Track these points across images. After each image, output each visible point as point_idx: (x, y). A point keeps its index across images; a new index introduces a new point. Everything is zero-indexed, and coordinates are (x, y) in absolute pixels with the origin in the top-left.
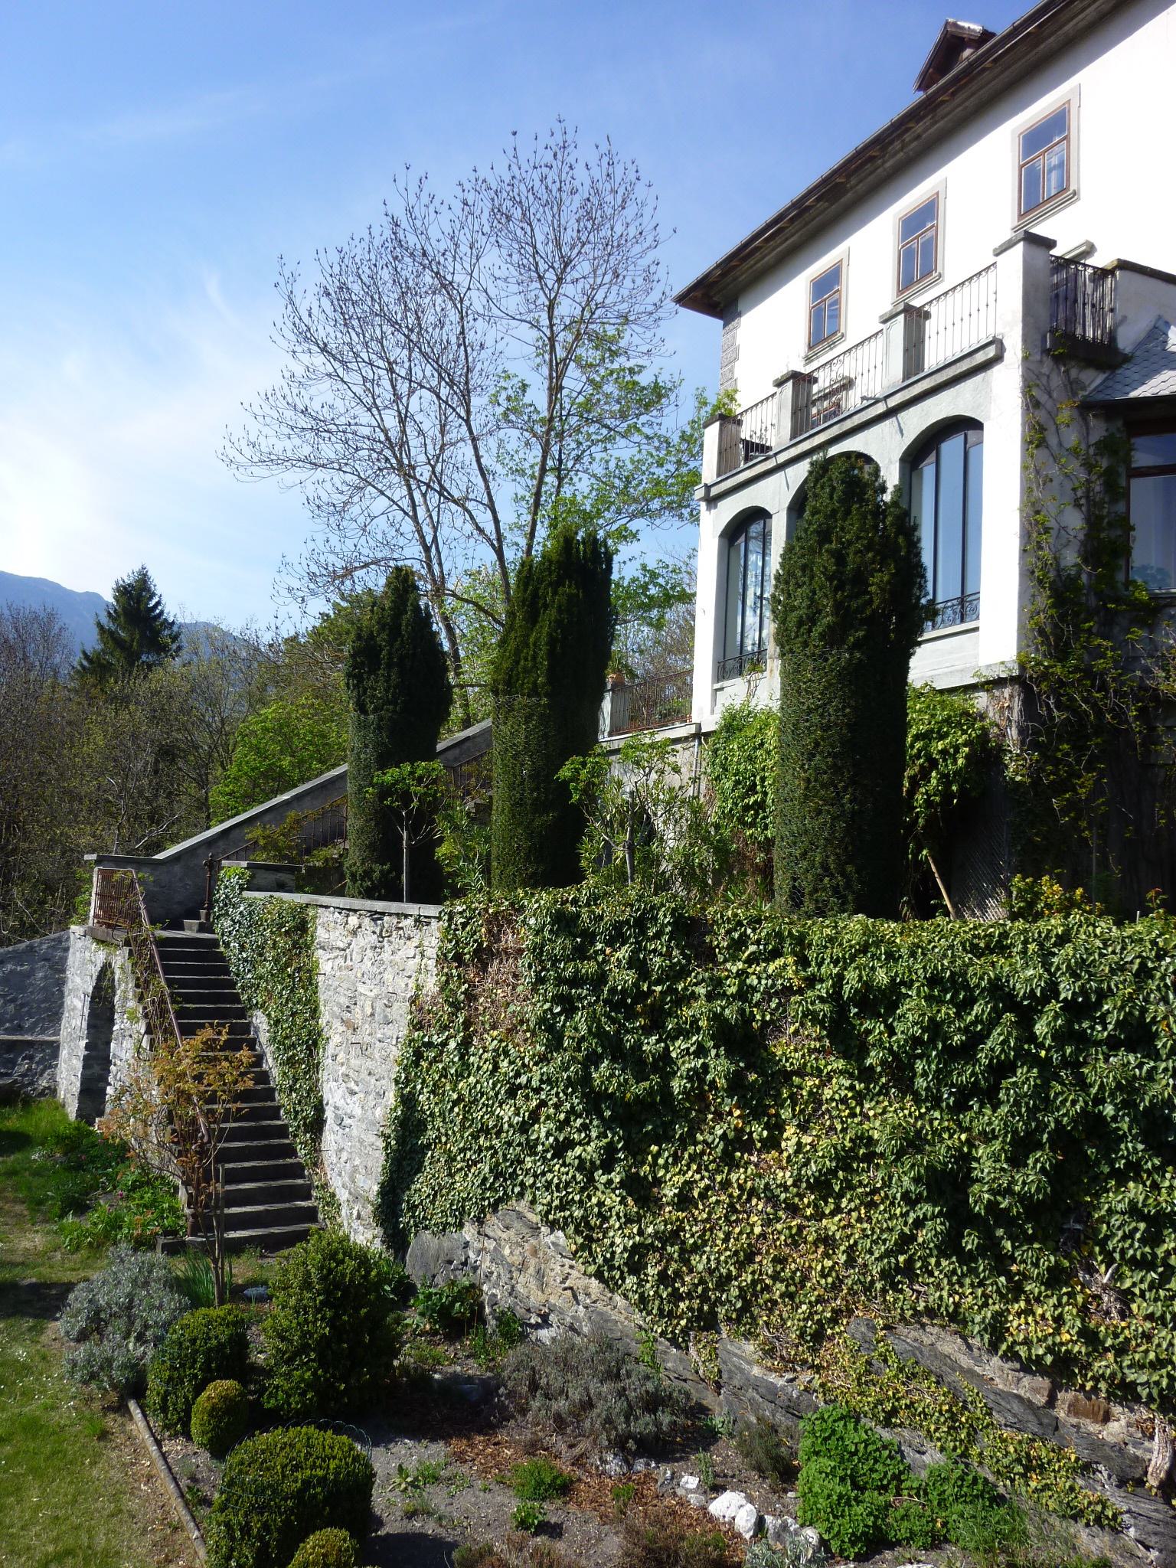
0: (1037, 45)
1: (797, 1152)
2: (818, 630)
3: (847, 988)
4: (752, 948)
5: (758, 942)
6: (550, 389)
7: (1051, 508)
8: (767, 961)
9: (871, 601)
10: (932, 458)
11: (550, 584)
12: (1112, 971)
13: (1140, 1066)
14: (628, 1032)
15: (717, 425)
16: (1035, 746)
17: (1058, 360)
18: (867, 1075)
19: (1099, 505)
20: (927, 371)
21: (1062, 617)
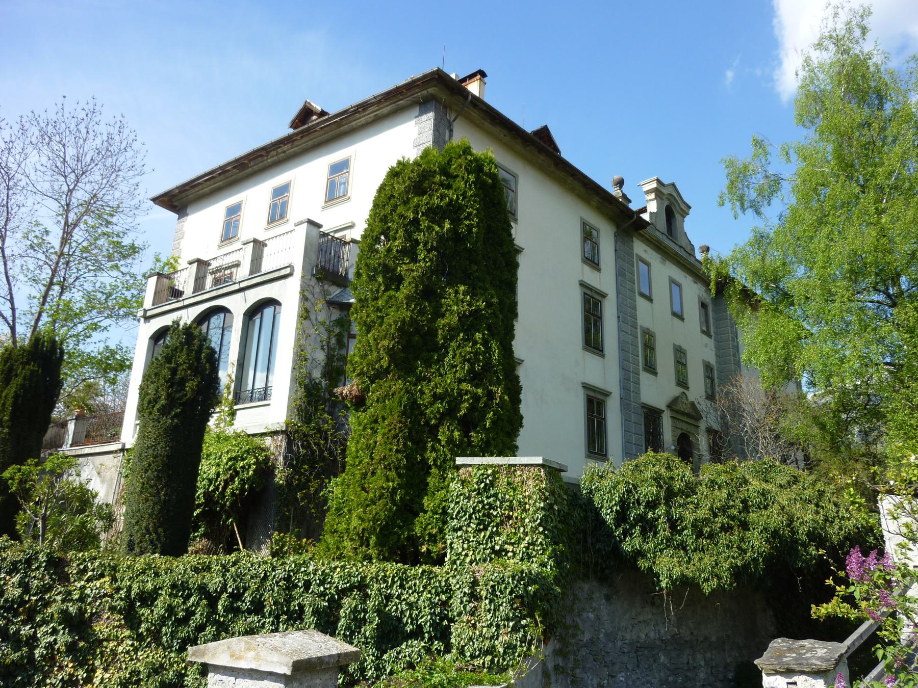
0: (340, 127)
1: (101, 683)
2: (157, 406)
3: (133, 592)
4: (90, 573)
5: (93, 570)
6: (63, 238)
7: (309, 349)
8: (98, 579)
9: (186, 395)
10: (259, 316)
11: (22, 363)
12: (252, 577)
13: (259, 622)
14: (13, 624)
15: (156, 277)
16: (291, 466)
17: (319, 279)
18: (140, 638)
19: (334, 350)
20: (264, 270)
21: (309, 403)
